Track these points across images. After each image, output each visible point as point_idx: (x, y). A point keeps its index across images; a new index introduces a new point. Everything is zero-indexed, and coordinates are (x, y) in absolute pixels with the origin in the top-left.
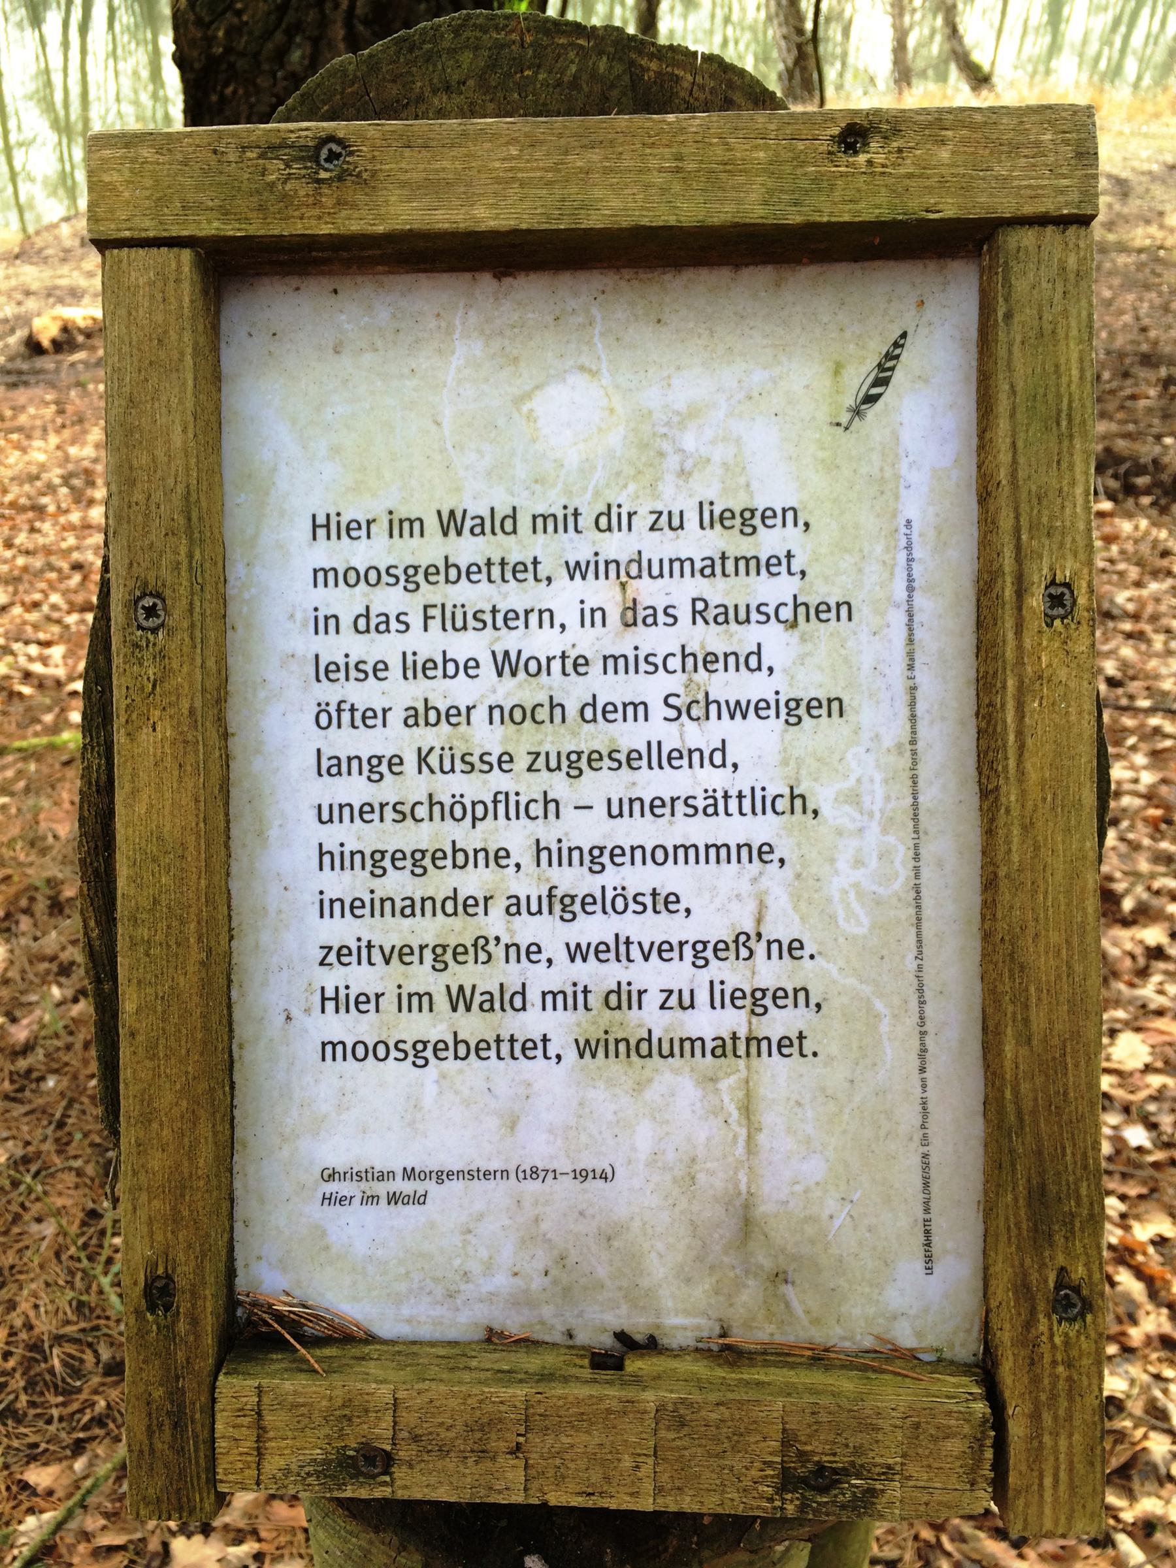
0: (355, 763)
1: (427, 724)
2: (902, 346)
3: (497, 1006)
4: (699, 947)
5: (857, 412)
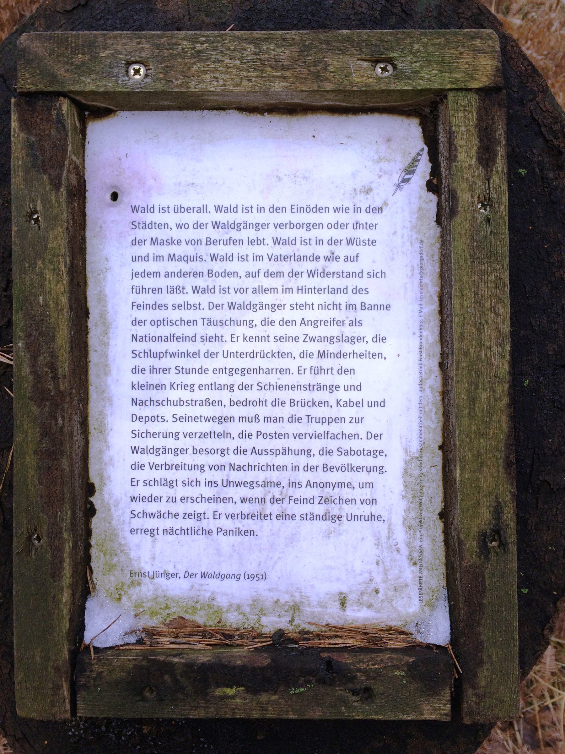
1: (181, 212)
2: (421, 155)
3: (226, 227)
4: (308, 225)
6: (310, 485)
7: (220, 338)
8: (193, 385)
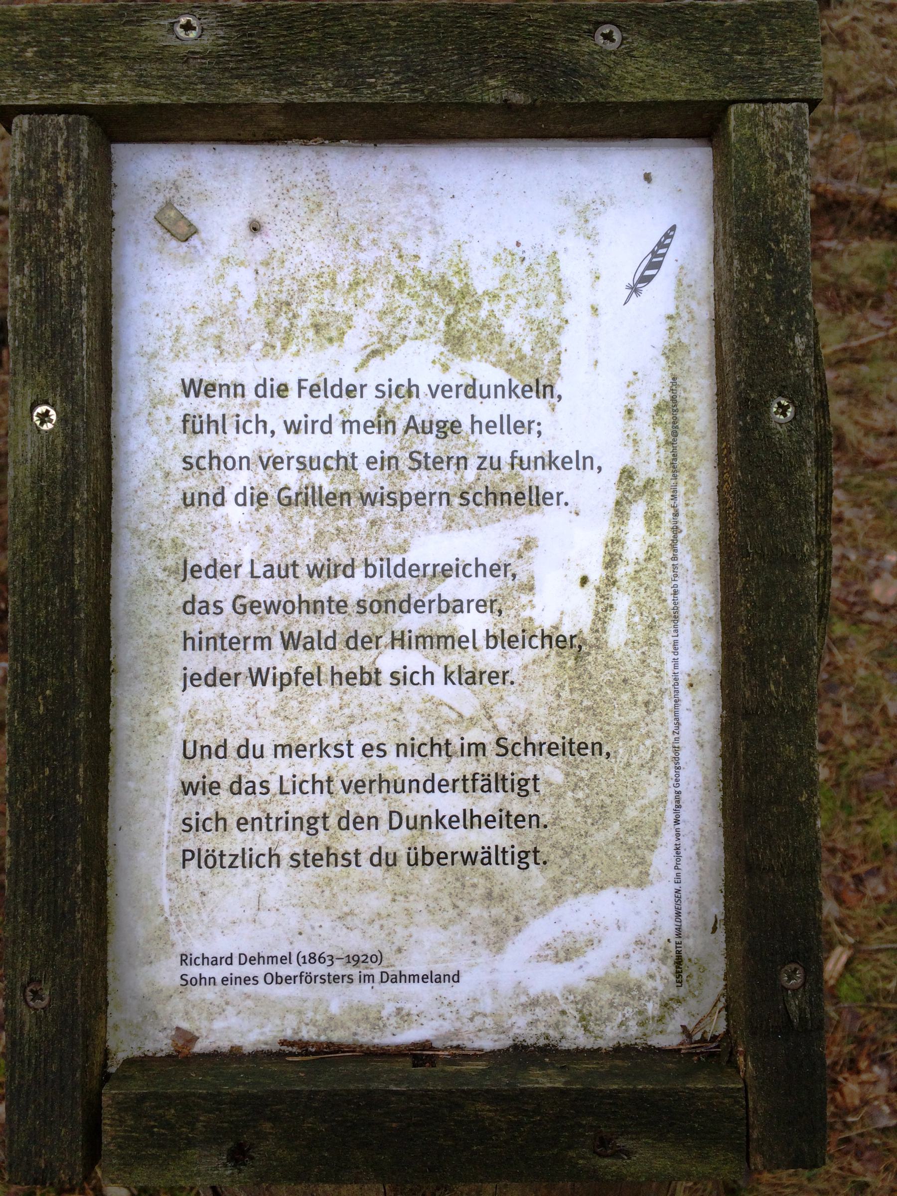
2: (672, 237)
3: (316, 645)
5: (634, 290)
6: (415, 427)
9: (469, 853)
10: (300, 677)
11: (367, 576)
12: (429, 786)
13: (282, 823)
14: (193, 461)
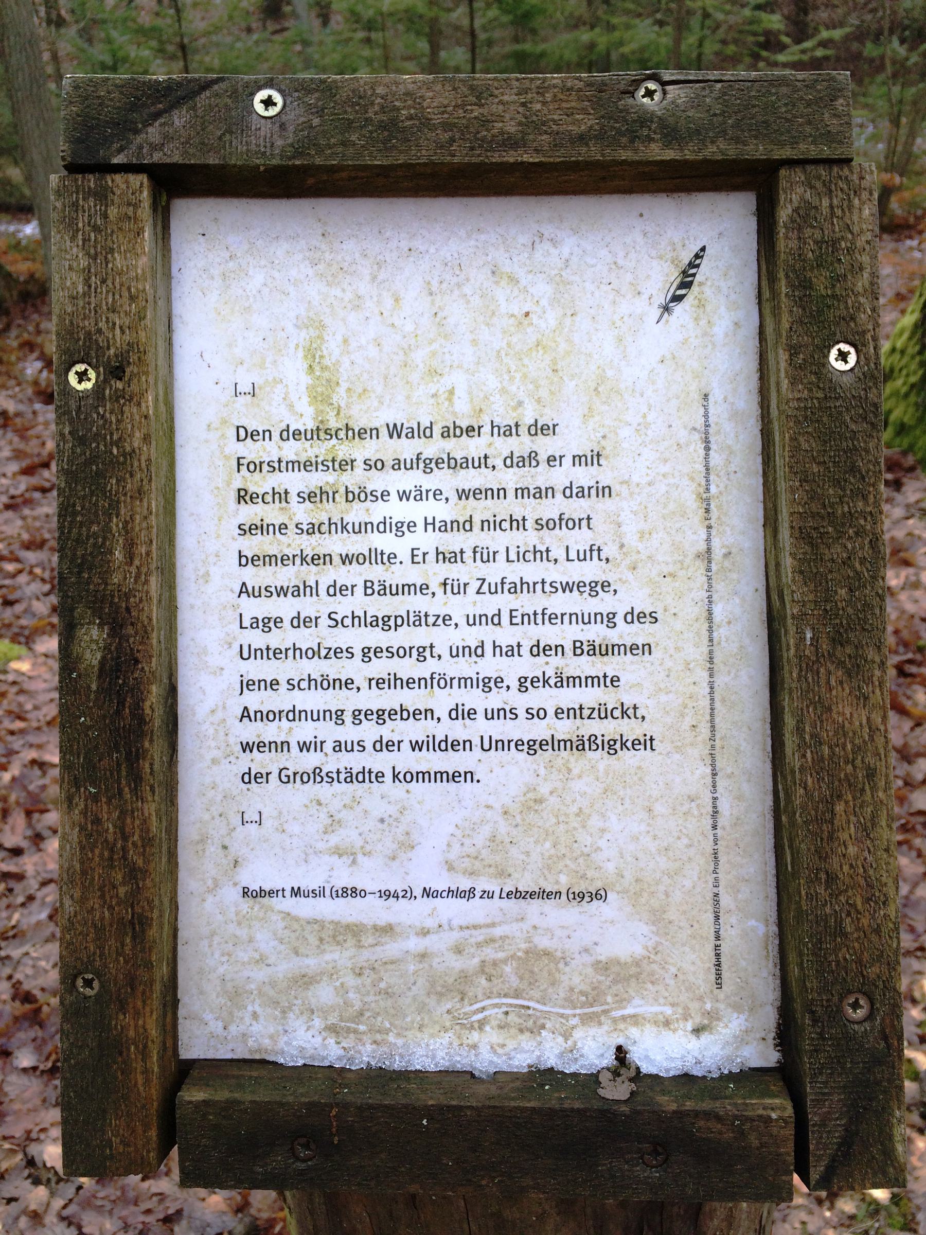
0: (328, 714)
5: (666, 309)
7: (545, 555)
8: (342, 711)
9: (395, 425)
10: (546, 617)
11: (347, 501)
12: (381, 528)
13: (593, 491)
14: (295, 683)
